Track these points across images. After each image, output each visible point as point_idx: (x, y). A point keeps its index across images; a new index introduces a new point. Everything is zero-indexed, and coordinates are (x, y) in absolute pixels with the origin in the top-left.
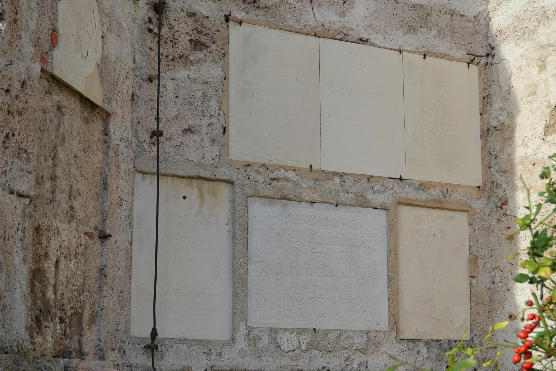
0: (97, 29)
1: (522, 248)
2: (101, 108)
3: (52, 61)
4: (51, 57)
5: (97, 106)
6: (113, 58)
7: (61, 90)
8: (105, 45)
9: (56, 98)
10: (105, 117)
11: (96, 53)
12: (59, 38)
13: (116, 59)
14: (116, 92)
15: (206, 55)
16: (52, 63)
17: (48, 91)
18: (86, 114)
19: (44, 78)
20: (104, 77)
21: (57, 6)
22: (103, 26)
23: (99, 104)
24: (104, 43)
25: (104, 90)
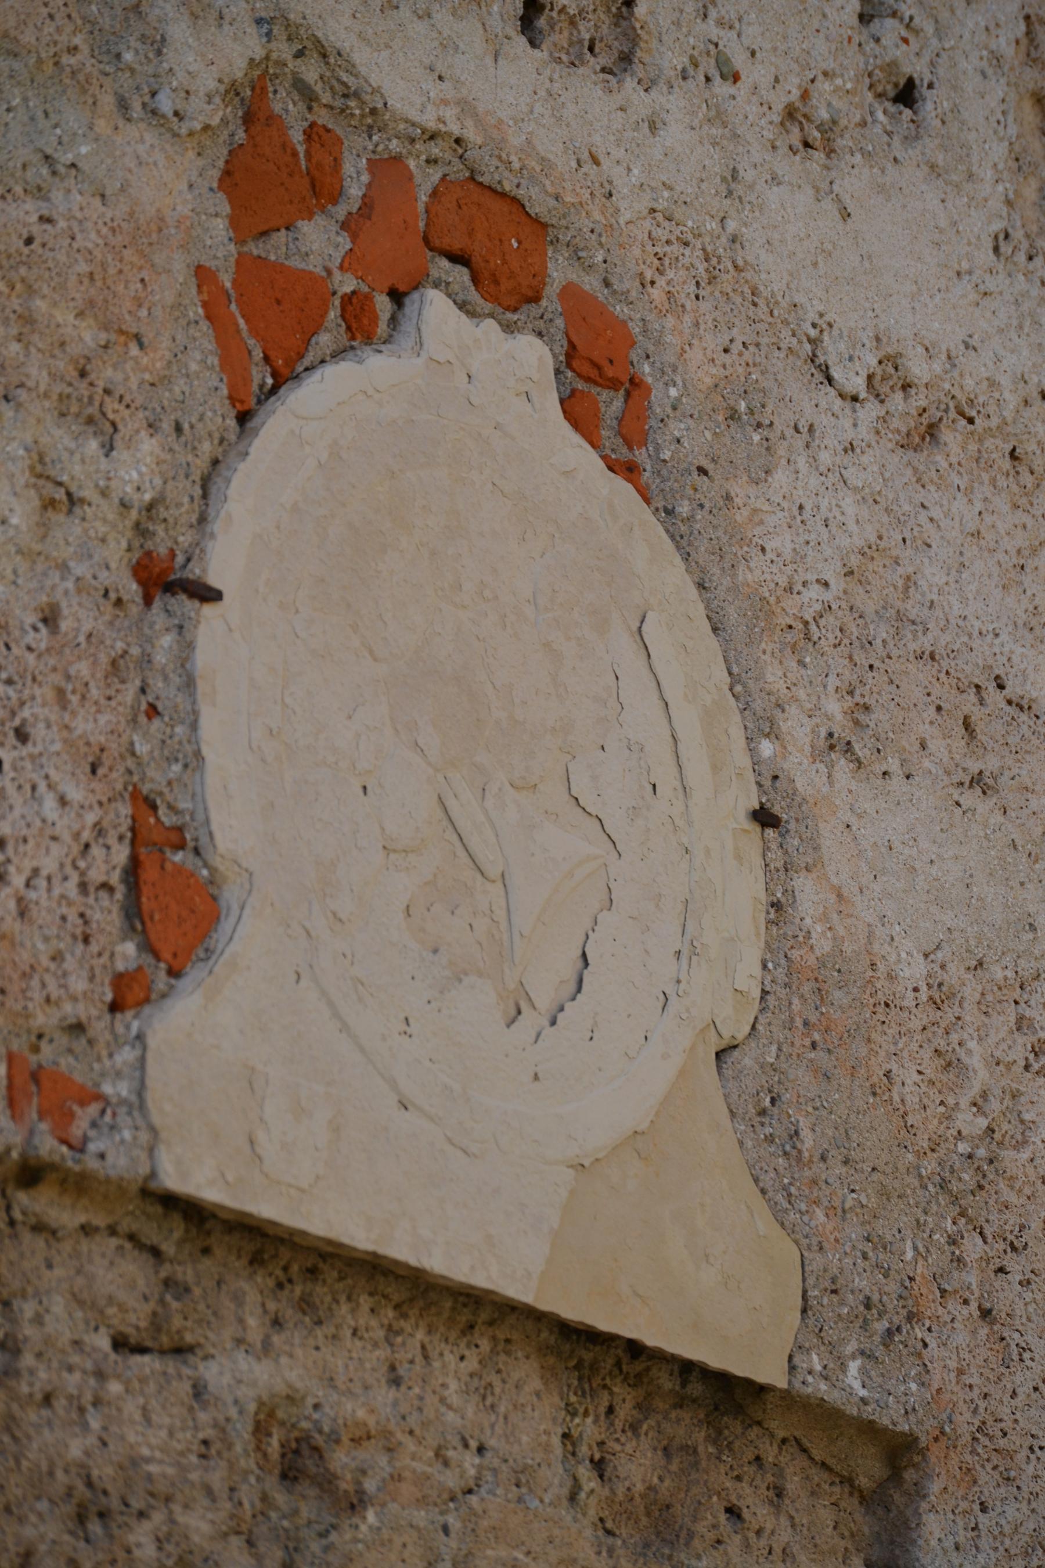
0: (698, 770)
1: (312, 83)
2: (789, 1399)
3: (140, 1091)
4: (126, 1055)
5: (761, 1390)
6: (914, 971)
7: (305, 1305)
8: (805, 886)
9: (242, 1373)
10: (869, 1469)
11: (688, 952)
12: (230, 895)
13: (955, 974)
14: (973, 1247)
15: (95, 577)
16: (139, 1103)
17: (157, 1324)
18: (638, 1466)
19: (87, 1230)
20: (808, 1141)
21: (188, 647)
22: (763, 726)
23: (770, 1373)
24: (780, 873)
25: (810, 1245)
